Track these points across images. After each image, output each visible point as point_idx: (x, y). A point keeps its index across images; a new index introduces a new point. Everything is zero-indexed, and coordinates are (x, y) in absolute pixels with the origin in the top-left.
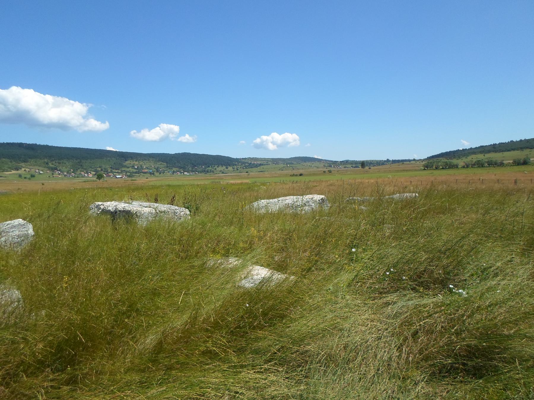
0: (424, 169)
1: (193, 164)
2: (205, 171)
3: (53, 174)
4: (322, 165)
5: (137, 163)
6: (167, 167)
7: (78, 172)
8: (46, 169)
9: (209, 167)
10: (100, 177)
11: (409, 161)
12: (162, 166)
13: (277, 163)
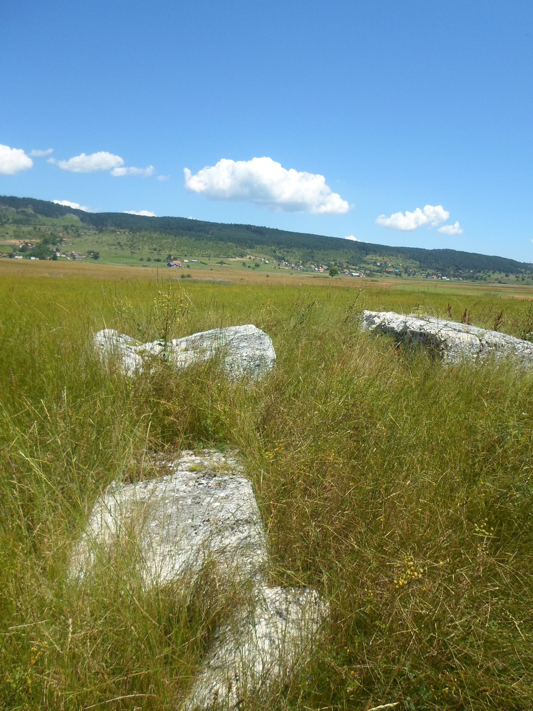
1: (456, 266)
2: (472, 277)
3: (279, 265)
5: (380, 258)
6: (420, 267)
8: (272, 258)
9: (480, 272)
10: (333, 273)
12: (413, 265)
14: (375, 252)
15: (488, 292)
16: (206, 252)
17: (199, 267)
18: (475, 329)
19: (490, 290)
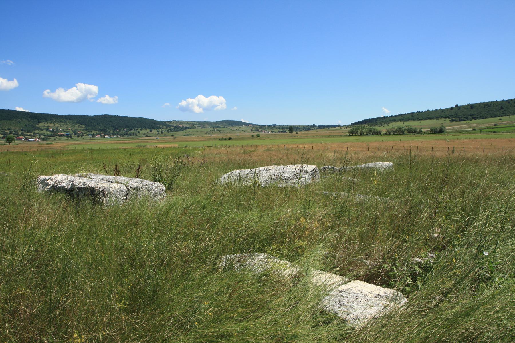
0: (350, 135)
1: (114, 127)
2: (127, 134)
4: (249, 129)
5: (52, 125)
6: (86, 130)
9: (131, 130)
11: (335, 126)
12: (80, 128)
15: (139, 144)
18: (122, 179)
19: (141, 143)
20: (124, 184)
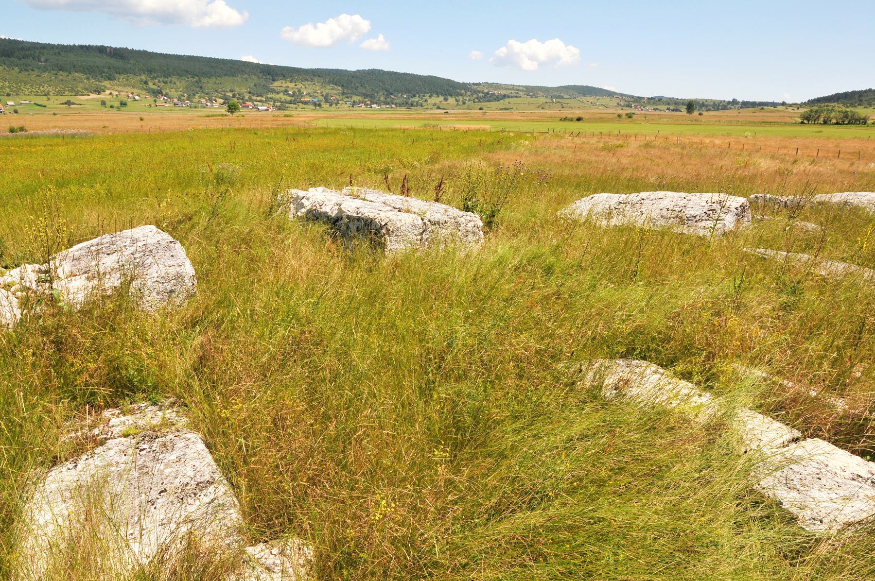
0: (802, 123)
1: (386, 91)
2: (407, 103)
3: (155, 101)
4: (614, 102)
5: (292, 85)
6: (343, 94)
7: (196, 99)
8: (144, 92)
9: (414, 96)
10: (232, 109)
11: (774, 105)
12: (334, 91)
13: (534, 96)
14: (284, 77)
15: (427, 122)
16: (42, 89)
17: (34, 112)
19: (428, 119)
20: (419, 215)
